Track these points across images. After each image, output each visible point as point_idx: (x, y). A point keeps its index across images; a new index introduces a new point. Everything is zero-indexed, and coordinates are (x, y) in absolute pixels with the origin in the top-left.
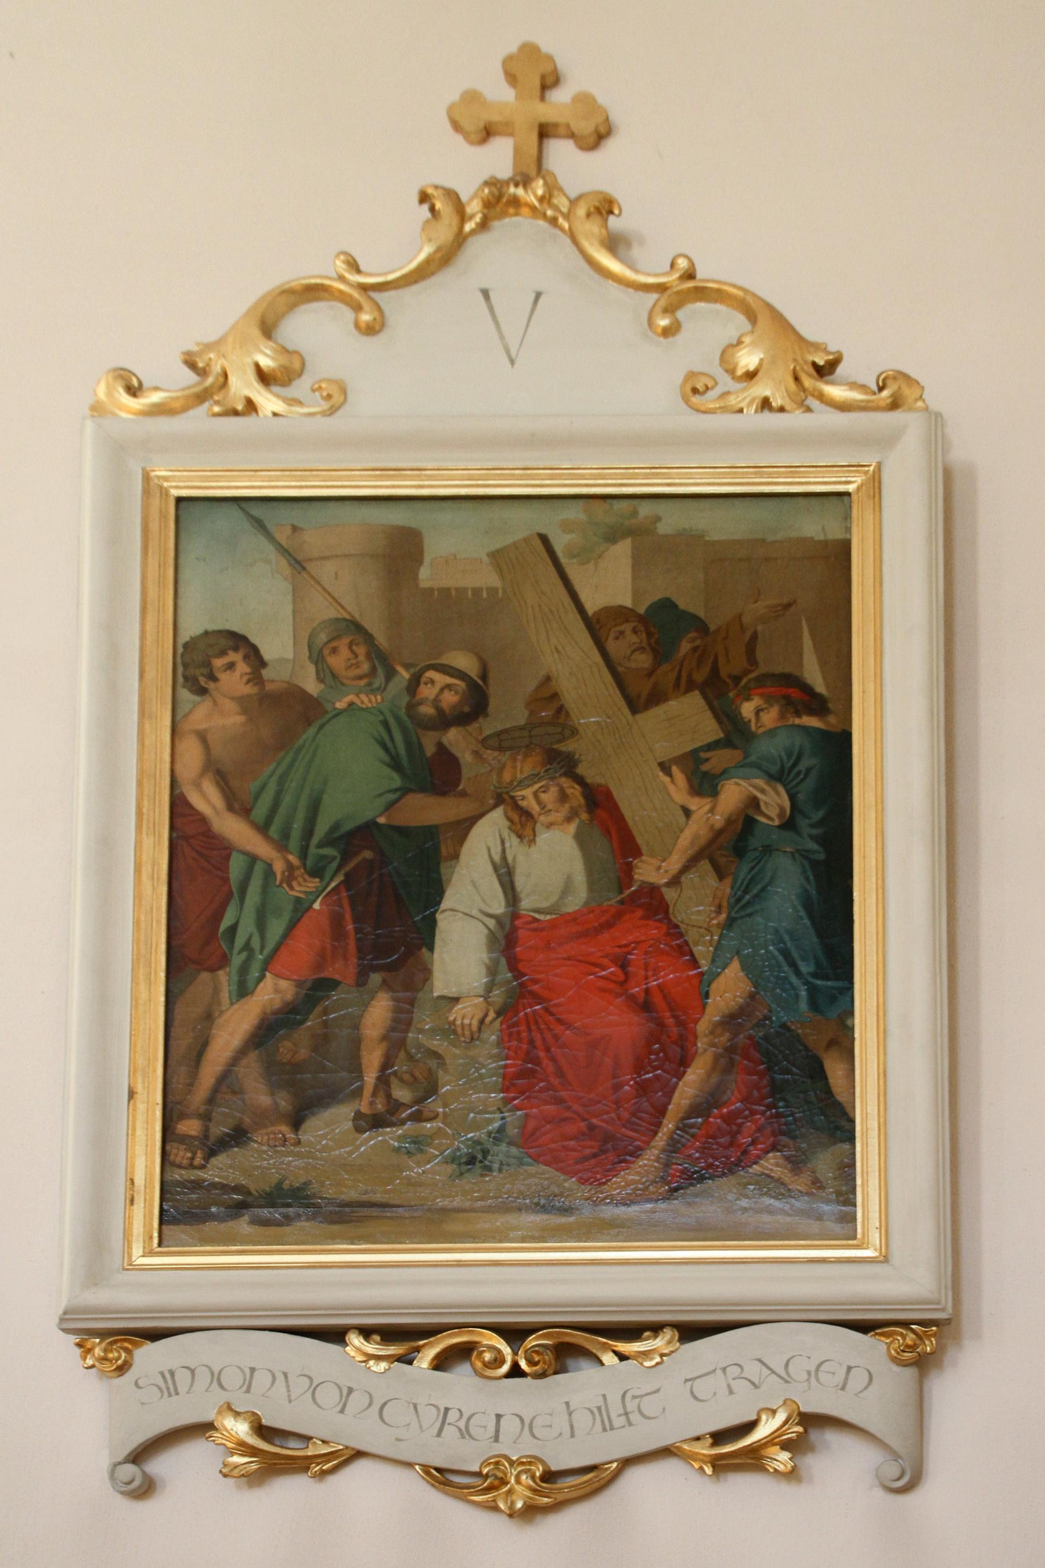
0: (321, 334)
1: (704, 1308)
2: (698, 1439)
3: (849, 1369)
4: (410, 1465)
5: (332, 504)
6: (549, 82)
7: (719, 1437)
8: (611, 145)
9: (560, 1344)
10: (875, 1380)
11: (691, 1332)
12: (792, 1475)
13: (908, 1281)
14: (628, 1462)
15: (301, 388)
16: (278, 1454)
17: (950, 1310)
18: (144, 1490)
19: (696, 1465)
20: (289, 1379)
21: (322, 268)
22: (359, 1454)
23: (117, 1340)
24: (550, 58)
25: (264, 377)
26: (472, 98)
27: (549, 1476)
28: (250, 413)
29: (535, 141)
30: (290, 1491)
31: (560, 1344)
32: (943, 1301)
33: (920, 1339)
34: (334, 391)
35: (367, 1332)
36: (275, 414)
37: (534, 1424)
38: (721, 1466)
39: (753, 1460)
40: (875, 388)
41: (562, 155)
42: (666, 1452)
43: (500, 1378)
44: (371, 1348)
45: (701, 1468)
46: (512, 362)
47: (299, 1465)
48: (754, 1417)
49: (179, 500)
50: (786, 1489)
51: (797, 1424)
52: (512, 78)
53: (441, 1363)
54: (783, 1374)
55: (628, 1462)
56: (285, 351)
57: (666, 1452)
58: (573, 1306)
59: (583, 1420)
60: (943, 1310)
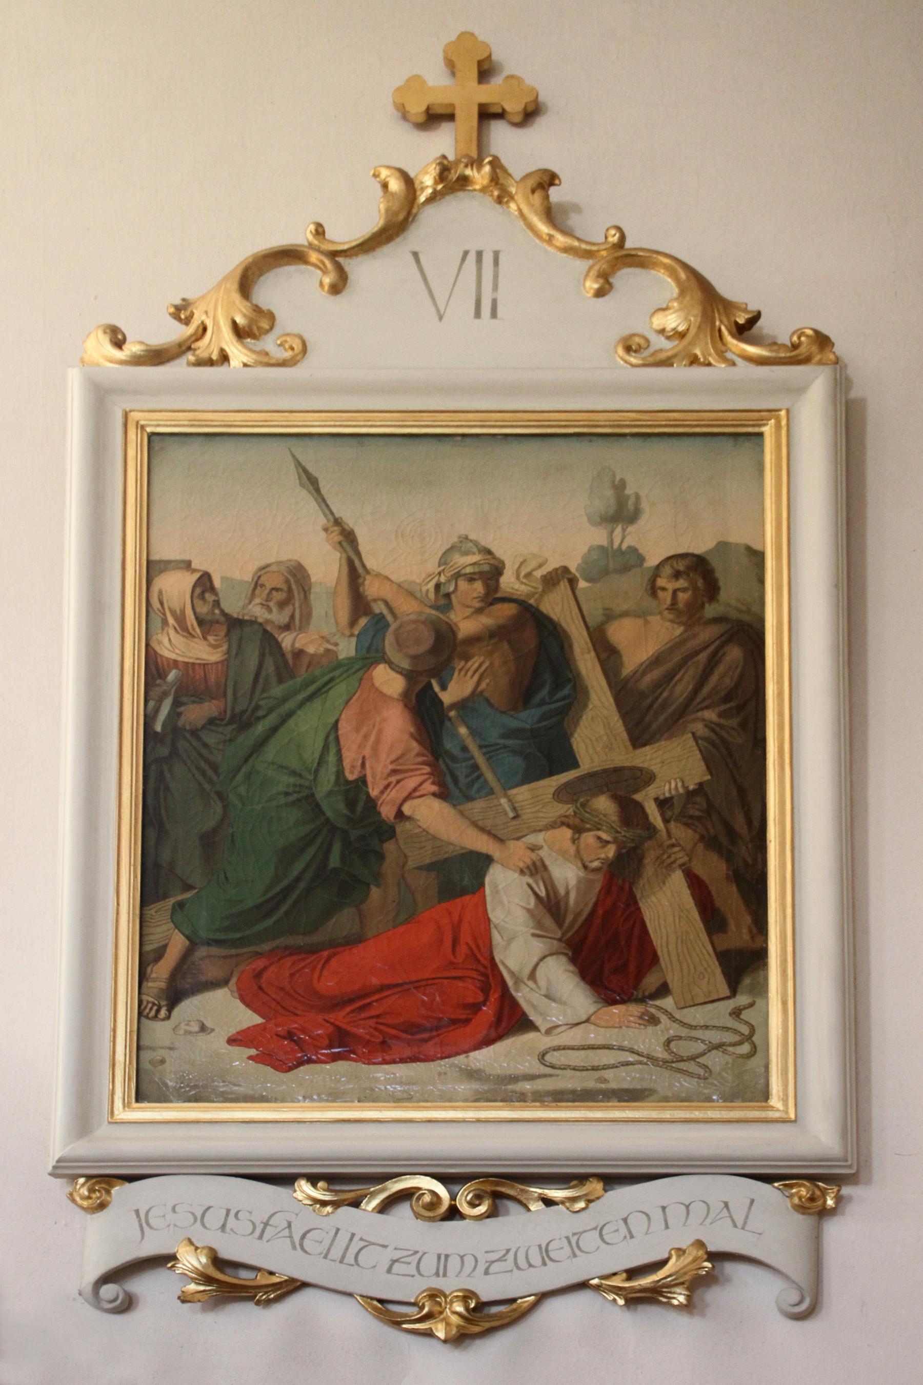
0: (294, 296)
1: (655, 1163)
3: (625, 1220)
4: (350, 1295)
8: (541, 124)
9: (501, 1186)
11: (611, 1180)
12: (689, 1307)
13: (818, 1135)
14: (543, 1297)
15: (269, 343)
16: (229, 1284)
17: (855, 1167)
19: (611, 1297)
20: (753, 1208)
22: (304, 1285)
23: (103, 1182)
25: (239, 333)
26: (415, 82)
27: (482, 1306)
28: (222, 364)
29: (479, 110)
32: (850, 1158)
33: (817, 1187)
34: (297, 346)
35: (313, 1179)
36: (245, 365)
38: (635, 1300)
39: (652, 1297)
41: (505, 140)
42: (583, 1285)
45: (614, 1300)
46: (441, 318)
48: (666, 1256)
49: (151, 435)
50: (683, 1320)
52: (451, 66)
53: (385, 1207)
55: (543, 1297)
56: (257, 310)
57: (583, 1285)
58: (650, 1160)
60: (850, 1167)
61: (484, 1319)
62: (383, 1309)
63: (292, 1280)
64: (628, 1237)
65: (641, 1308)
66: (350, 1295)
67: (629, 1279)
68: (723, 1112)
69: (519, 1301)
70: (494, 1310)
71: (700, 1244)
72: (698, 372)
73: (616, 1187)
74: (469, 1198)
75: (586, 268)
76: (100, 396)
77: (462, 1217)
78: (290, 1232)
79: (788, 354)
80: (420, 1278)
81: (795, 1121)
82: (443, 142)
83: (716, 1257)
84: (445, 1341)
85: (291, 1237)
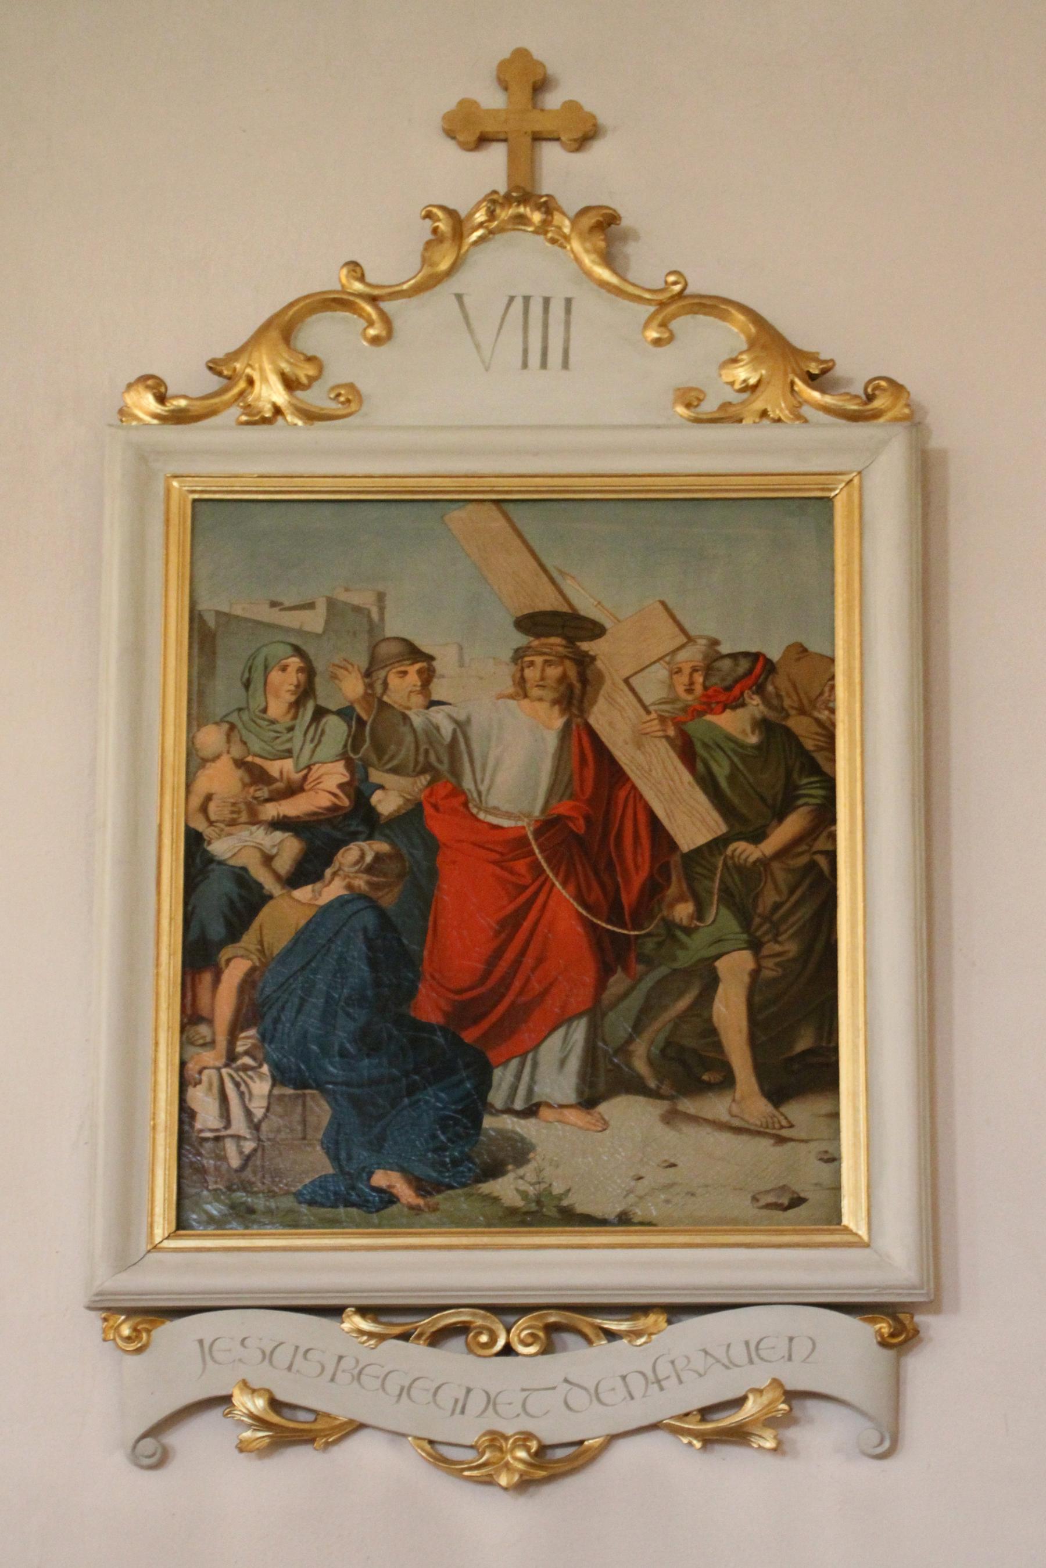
2: (687, 1415)
5: (295, 505)
6: (540, 86)
7: (705, 1413)
8: (599, 149)
9: (564, 1322)
10: (564, 1408)
11: (676, 1311)
13: (891, 1261)
14: (613, 1438)
16: (289, 1428)
18: (161, 1461)
19: (685, 1440)
21: (333, 278)
24: (541, 64)
27: (543, 1449)
29: (524, 118)
30: (299, 1460)
31: (564, 1322)
33: (896, 1322)
35: (363, 1311)
37: (600, 1391)
38: (709, 1440)
39: (739, 1435)
40: (864, 397)
41: (553, 158)
43: (490, 1356)
44: (365, 1325)
45: (690, 1444)
47: (303, 1438)
50: (771, 1460)
51: (783, 1402)
54: (725, 1361)
55: (613, 1438)
57: (654, 1427)
59: (637, 1383)
61: (551, 1464)
62: (436, 1454)
63: (351, 1421)
64: (628, 1398)
65: (718, 1448)
66: (404, 1435)
67: (703, 1420)
68: (510, 1127)
69: (586, 1443)
70: (560, 1453)
71: (776, 1382)
72: (768, 432)
73: (681, 1317)
74: (523, 1334)
75: (647, 315)
76: (143, 459)
77: (517, 1354)
78: (711, 1355)
79: (861, 408)
80: (601, 1407)
81: (867, 1245)
82: (491, 168)
83: (791, 1396)
84: (505, 1489)
85: (718, 1361)
